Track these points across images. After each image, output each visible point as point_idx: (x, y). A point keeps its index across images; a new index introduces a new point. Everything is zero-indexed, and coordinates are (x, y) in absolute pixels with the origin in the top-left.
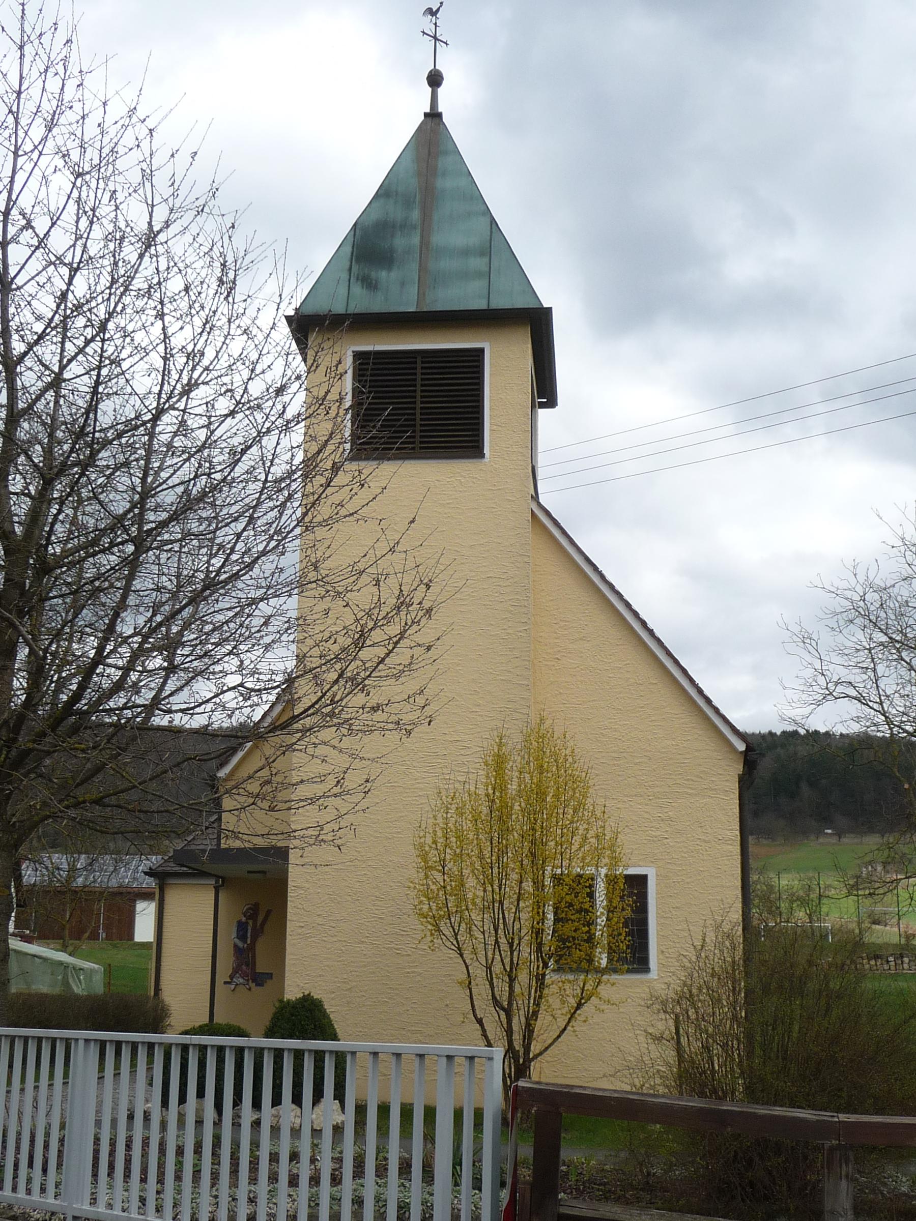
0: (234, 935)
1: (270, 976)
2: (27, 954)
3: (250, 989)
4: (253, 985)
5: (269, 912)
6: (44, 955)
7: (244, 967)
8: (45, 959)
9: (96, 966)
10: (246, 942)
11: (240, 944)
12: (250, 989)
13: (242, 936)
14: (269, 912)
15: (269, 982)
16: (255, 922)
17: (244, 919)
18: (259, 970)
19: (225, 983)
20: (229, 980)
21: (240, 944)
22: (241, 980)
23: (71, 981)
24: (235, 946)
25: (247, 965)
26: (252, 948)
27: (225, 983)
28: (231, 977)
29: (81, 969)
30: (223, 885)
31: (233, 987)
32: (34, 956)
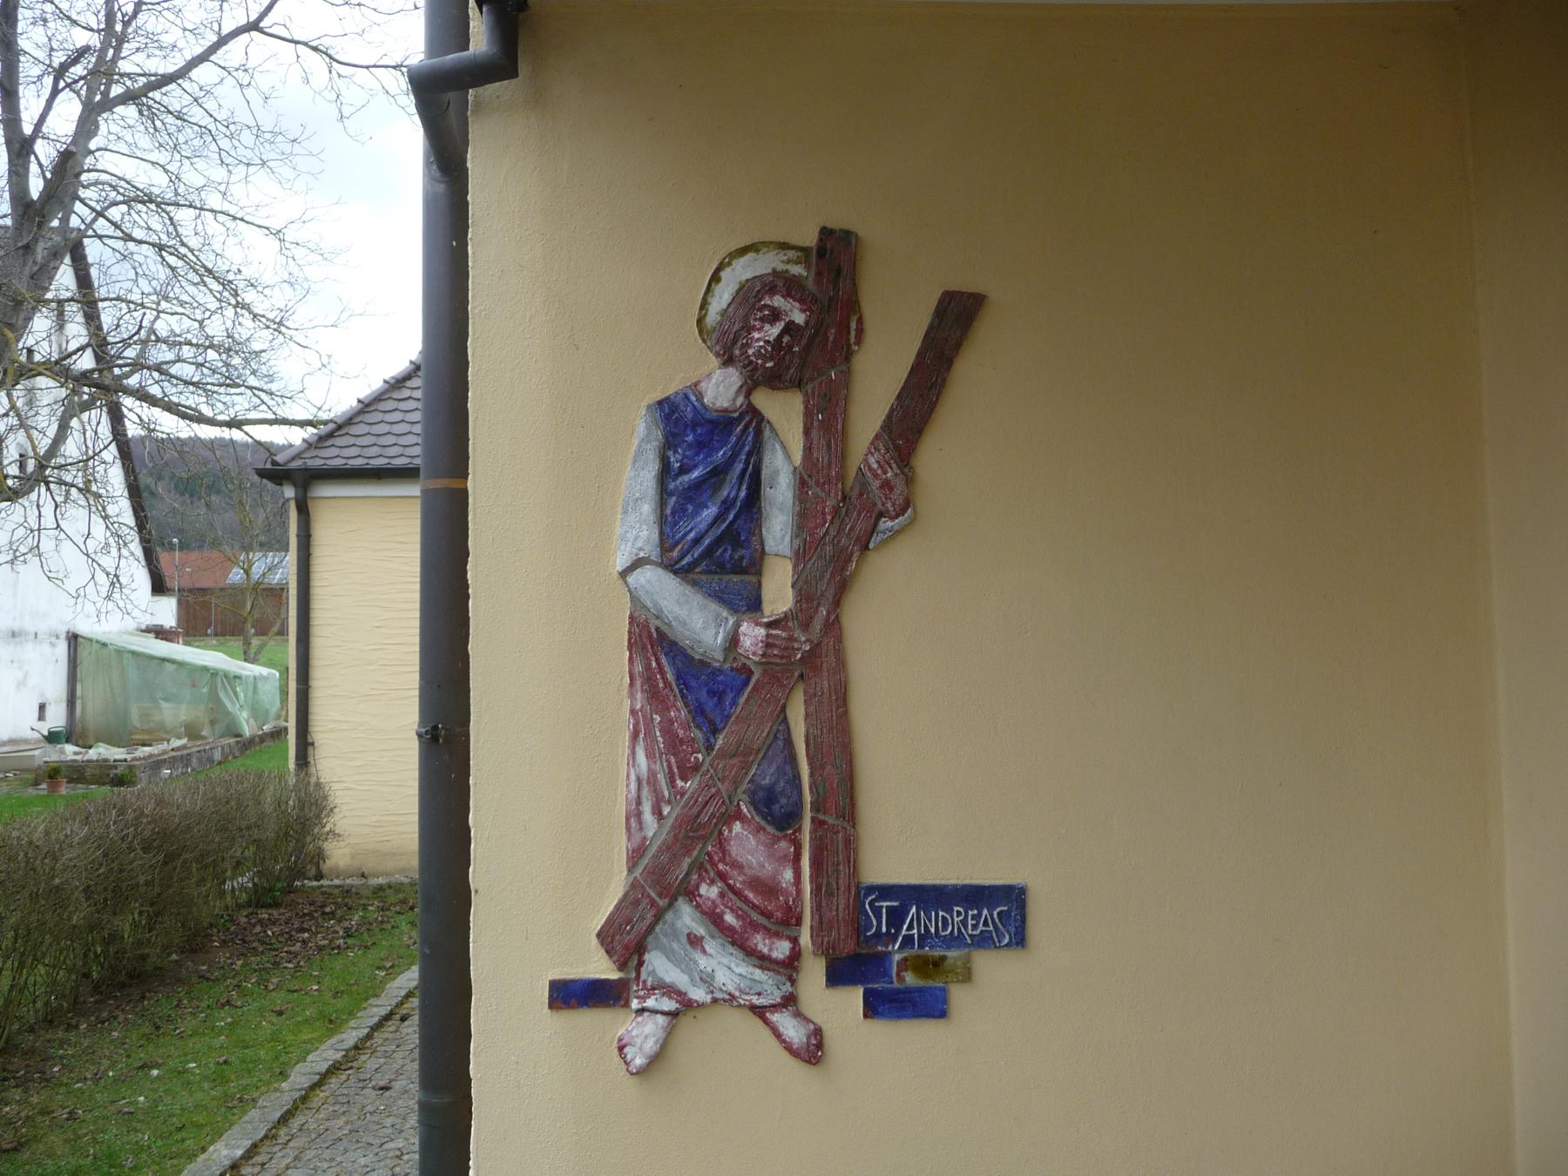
0: (635, 529)
1: (1002, 912)
2: (151, 658)
3: (813, 1052)
4: (838, 1009)
5: (956, 317)
6: (178, 657)
7: (747, 845)
8: (181, 665)
9: (265, 671)
10: (754, 605)
11: (699, 622)
12: (813, 1052)
13: (718, 555)
14: (956, 317)
15: (994, 969)
16: (827, 419)
17: (720, 388)
18: (895, 854)
19: (571, 995)
20: (602, 968)
21: (699, 622)
22: (726, 969)
23: (222, 695)
24: (652, 641)
25: (778, 814)
26: (812, 655)
27: (571, 995)
28: (627, 938)
29: (236, 677)
30: (501, 67)
31: (644, 1033)
32: (164, 660)
